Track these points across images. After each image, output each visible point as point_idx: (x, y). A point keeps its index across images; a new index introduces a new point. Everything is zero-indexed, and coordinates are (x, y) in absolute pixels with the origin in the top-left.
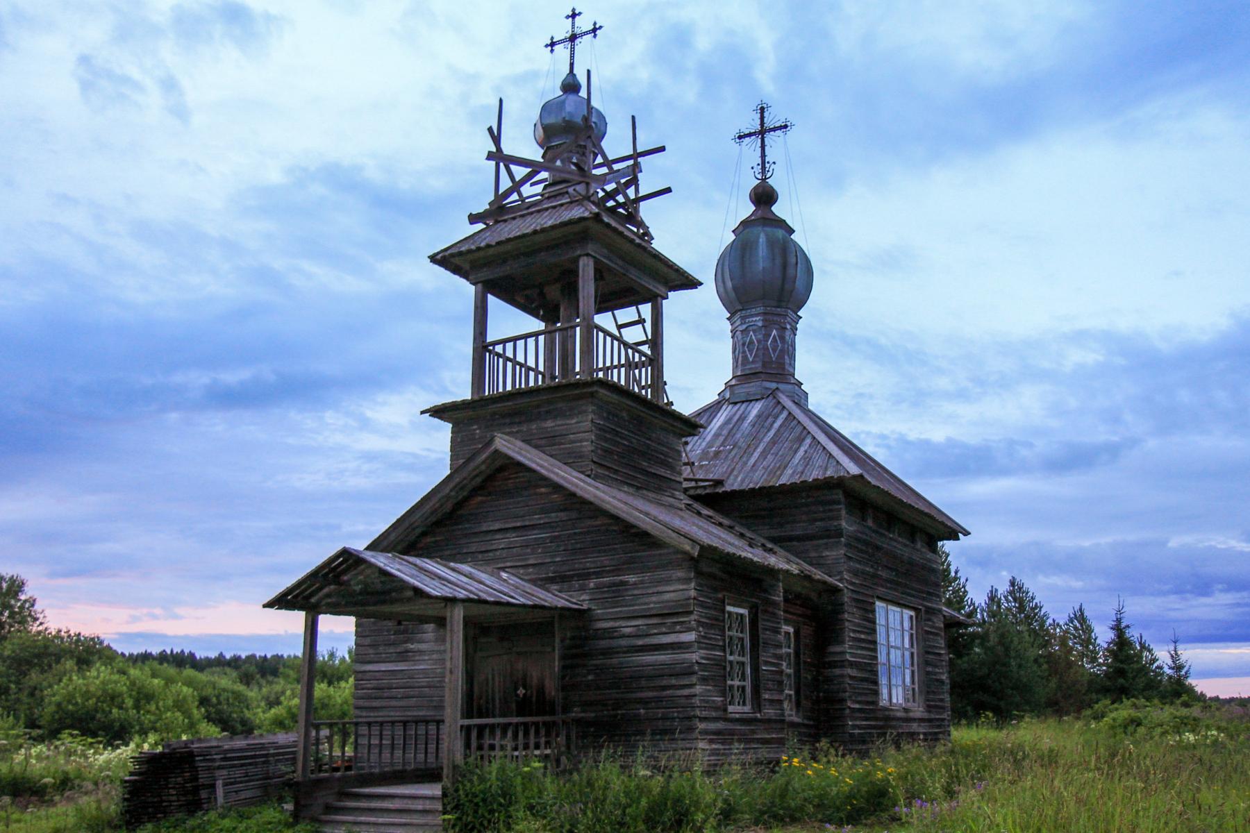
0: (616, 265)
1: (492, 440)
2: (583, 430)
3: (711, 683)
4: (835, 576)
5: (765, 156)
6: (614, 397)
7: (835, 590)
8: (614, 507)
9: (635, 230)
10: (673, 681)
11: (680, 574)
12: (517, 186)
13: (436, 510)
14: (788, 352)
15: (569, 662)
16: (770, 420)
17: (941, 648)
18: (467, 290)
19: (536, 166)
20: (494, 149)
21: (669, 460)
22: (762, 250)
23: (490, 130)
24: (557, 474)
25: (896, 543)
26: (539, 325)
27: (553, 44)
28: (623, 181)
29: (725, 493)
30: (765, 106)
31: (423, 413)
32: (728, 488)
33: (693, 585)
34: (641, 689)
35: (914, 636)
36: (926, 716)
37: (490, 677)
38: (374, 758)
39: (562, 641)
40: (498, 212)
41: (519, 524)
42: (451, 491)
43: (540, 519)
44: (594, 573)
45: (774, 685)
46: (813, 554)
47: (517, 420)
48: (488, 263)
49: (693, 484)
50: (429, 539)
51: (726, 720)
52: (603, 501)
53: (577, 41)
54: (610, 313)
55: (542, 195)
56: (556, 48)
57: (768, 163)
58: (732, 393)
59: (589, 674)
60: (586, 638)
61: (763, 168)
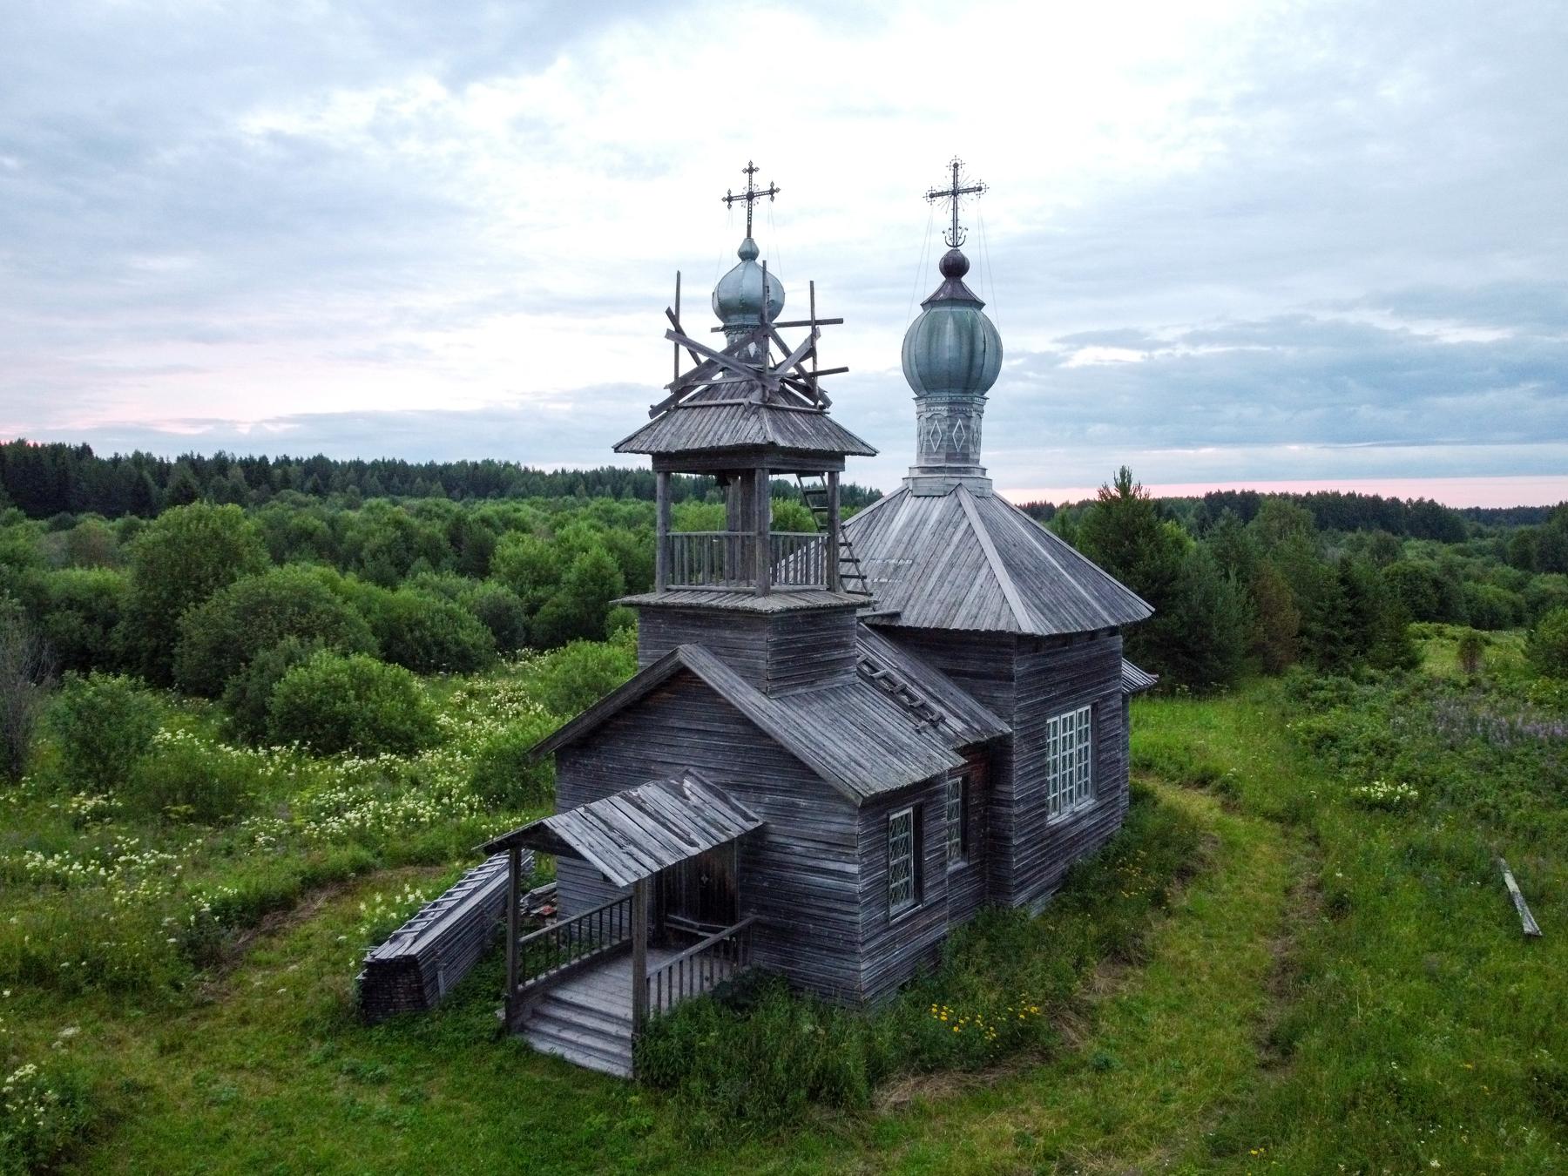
1: (674, 653)
10: (838, 906)
15: (747, 866)
16: (951, 529)
20: (673, 329)
22: (949, 338)
23: (669, 312)
27: (730, 199)
29: (901, 628)
32: (901, 623)
34: (810, 906)
36: (1098, 804)
41: (701, 727)
44: (769, 789)
50: (621, 722)
53: (755, 200)
56: (733, 203)
58: (915, 485)
60: (762, 848)
61: (955, 233)
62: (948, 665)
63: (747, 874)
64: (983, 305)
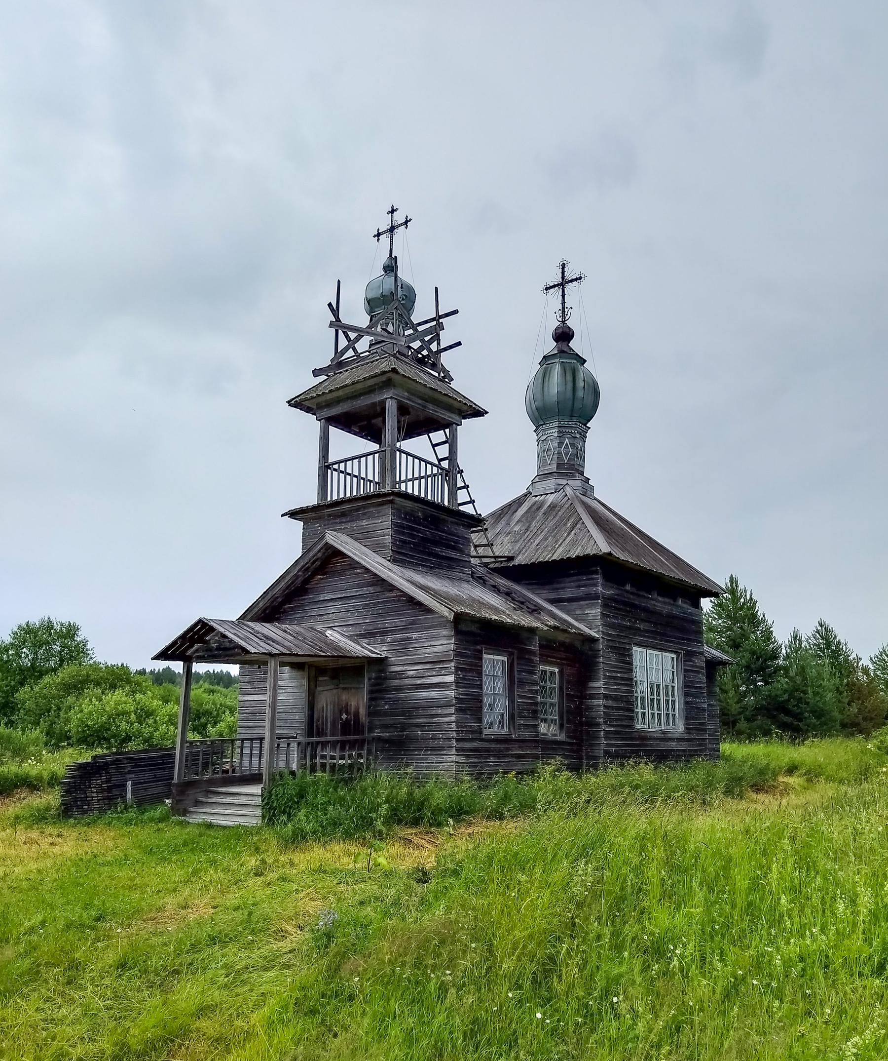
0: (414, 403)
1: (323, 537)
2: (385, 527)
3: (468, 712)
4: (594, 629)
5: (565, 303)
6: (408, 504)
7: (594, 640)
8: (401, 584)
9: (436, 374)
11: (445, 632)
12: (351, 344)
13: (290, 585)
14: (580, 454)
15: (374, 695)
17: (703, 683)
18: (311, 424)
19: (361, 331)
21: (459, 545)
23: (330, 305)
24: (365, 560)
25: (660, 604)
26: (375, 447)
28: (427, 339)
30: (565, 262)
31: (283, 515)
32: (516, 562)
33: (453, 641)
35: (675, 673)
36: (686, 736)
37: (325, 706)
38: (246, 763)
39: (370, 679)
40: (338, 365)
42: (298, 572)
43: (357, 591)
45: (529, 713)
46: (578, 612)
47: (344, 520)
48: (329, 405)
49: (493, 560)
51: (482, 740)
52: (393, 579)
54: (442, 431)
55: (369, 352)
57: (567, 308)
59: (386, 704)
62: (553, 596)
63: (373, 703)
64: (585, 361)
